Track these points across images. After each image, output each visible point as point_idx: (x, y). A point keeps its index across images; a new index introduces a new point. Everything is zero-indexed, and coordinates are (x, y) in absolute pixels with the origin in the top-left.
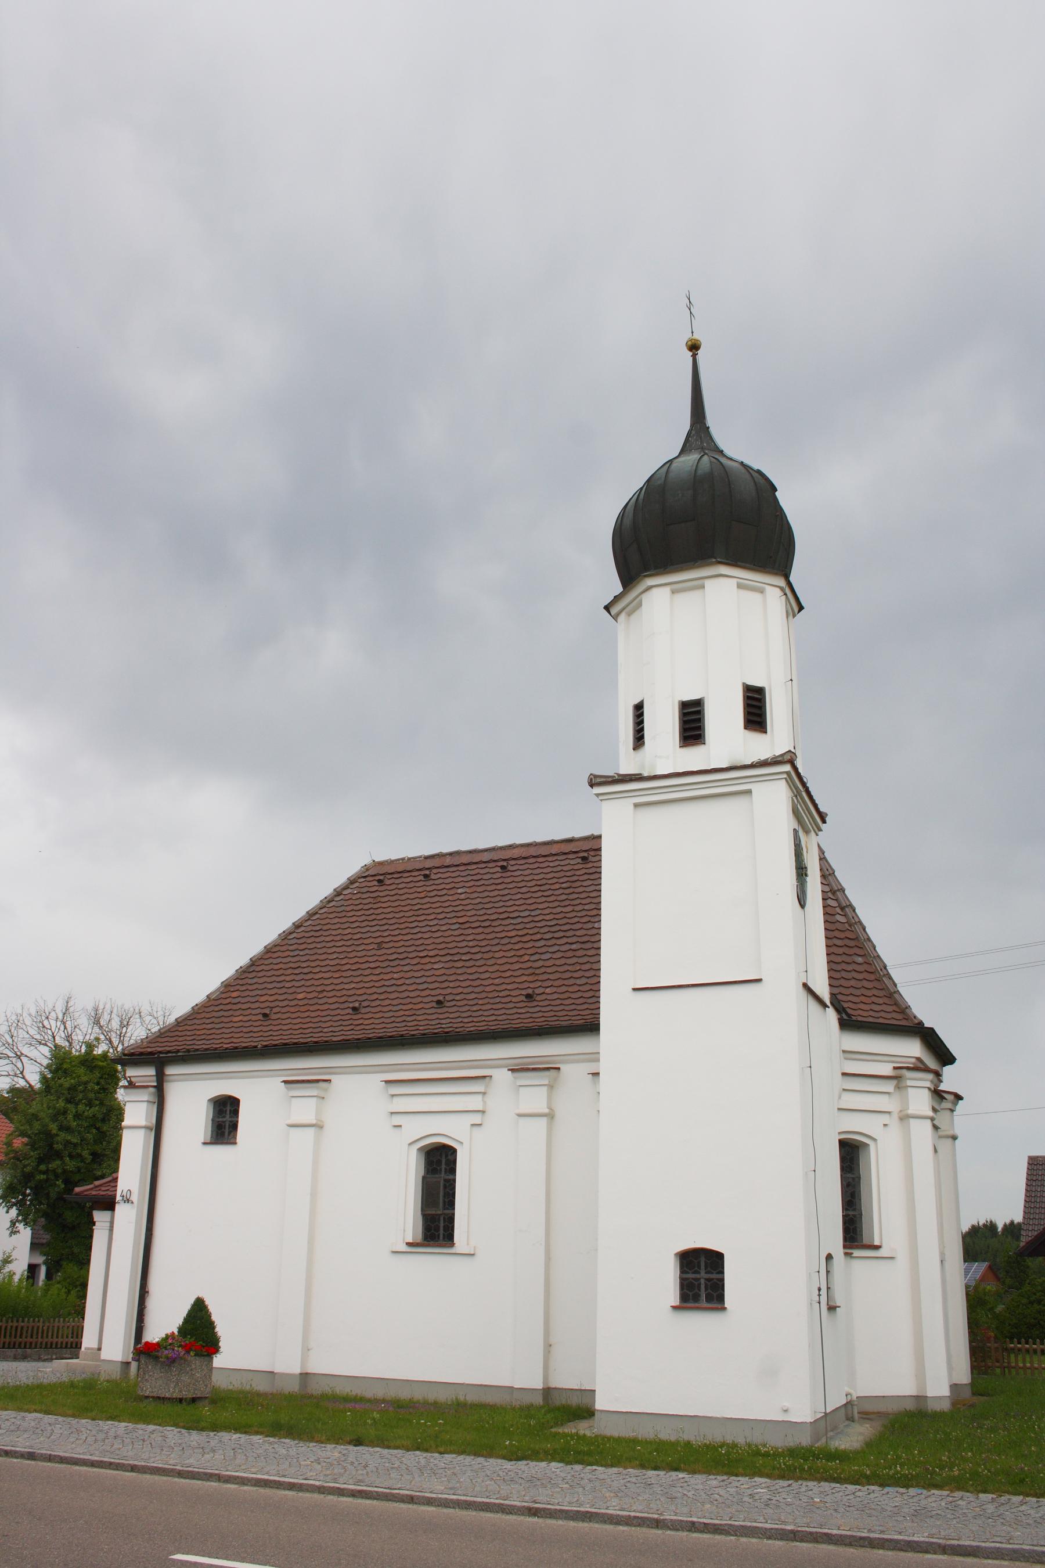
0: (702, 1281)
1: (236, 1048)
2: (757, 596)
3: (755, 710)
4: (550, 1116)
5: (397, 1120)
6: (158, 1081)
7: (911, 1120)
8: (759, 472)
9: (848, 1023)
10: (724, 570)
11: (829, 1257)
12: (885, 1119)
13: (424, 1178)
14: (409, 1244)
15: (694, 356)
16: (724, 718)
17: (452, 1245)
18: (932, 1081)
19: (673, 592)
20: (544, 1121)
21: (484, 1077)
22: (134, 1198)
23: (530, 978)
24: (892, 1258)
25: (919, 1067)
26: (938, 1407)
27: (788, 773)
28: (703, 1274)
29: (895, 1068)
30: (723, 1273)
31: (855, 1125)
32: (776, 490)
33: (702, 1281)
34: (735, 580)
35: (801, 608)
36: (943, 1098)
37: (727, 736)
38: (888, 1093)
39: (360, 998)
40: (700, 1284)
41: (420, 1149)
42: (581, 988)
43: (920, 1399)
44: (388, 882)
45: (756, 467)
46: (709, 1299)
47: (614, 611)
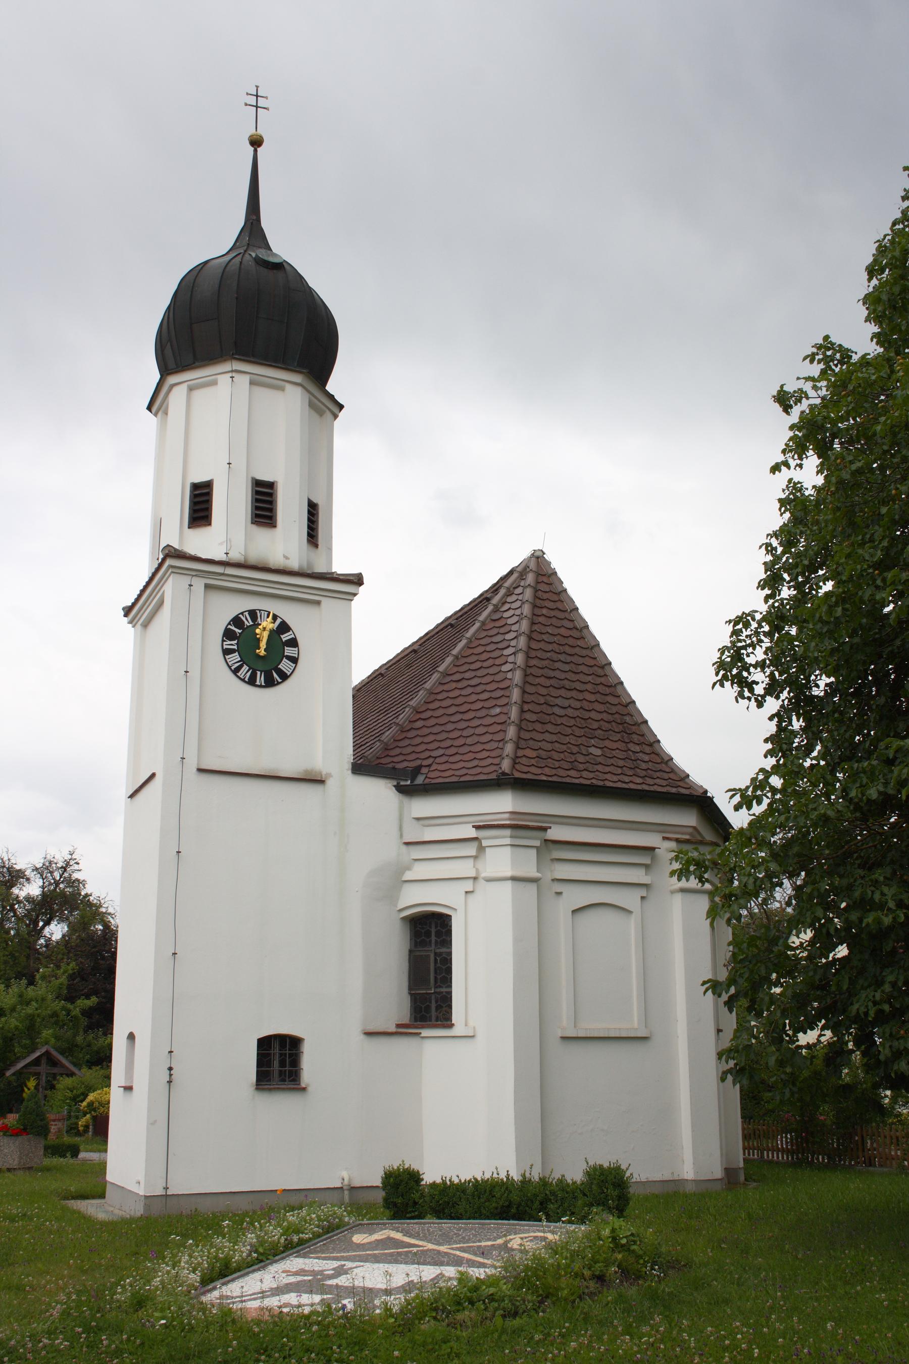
3: (263, 504)
5: (558, 887)
13: (410, 951)
15: (256, 151)
16: (231, 504)
17: (451, 1026)
24: (645, 1039)
31: (418, 898)
34: (186, 384)
42: (485, 746)
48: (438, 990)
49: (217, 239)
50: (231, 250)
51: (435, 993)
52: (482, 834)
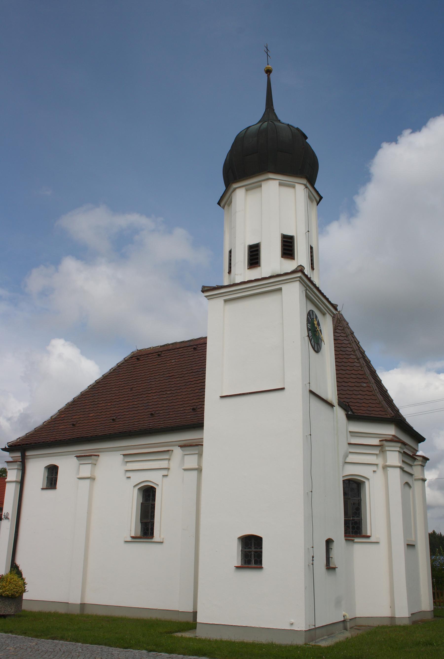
0: (253, 553)
1: (56, 441)
2: (291, 190)
3: (288, 247)
4: (199, 470)
5: (129, 474)
6: (22, 459)
7: (388, 469)
8: (298, 129)
9: (352, 417)
10: (271, 176)
11: (329, 542)
12: (374, 468)
13: (142, 504)
14: (133, 537)
18: (400, 447)
19: (247, 190)
20: (195, 473)
21: (168, 451)
22: (10, 517)
23: (197, 401)
25: (394, 440)
26: (403, 623)
27: (300, 277)
28: (253, 549)
29: (380, 441)
30: (262, 548)
31: (352, 471)
32: (306, 138)
33: (253, 553)
35: (321, 198)
36: (415, 459)
37: (272, 261)
38: (376, 454)
39: (117, 415)
40: (251, 555)
41: (139, 489)
43: (392, 618)
44: (142, 359)
45: (296, 126)
46: (256, 563)
47: (222, 205)
48: (354, 518)
49: (251, 116)
50: (257, 124)
51: (353, 520)
52: (384, 443)
